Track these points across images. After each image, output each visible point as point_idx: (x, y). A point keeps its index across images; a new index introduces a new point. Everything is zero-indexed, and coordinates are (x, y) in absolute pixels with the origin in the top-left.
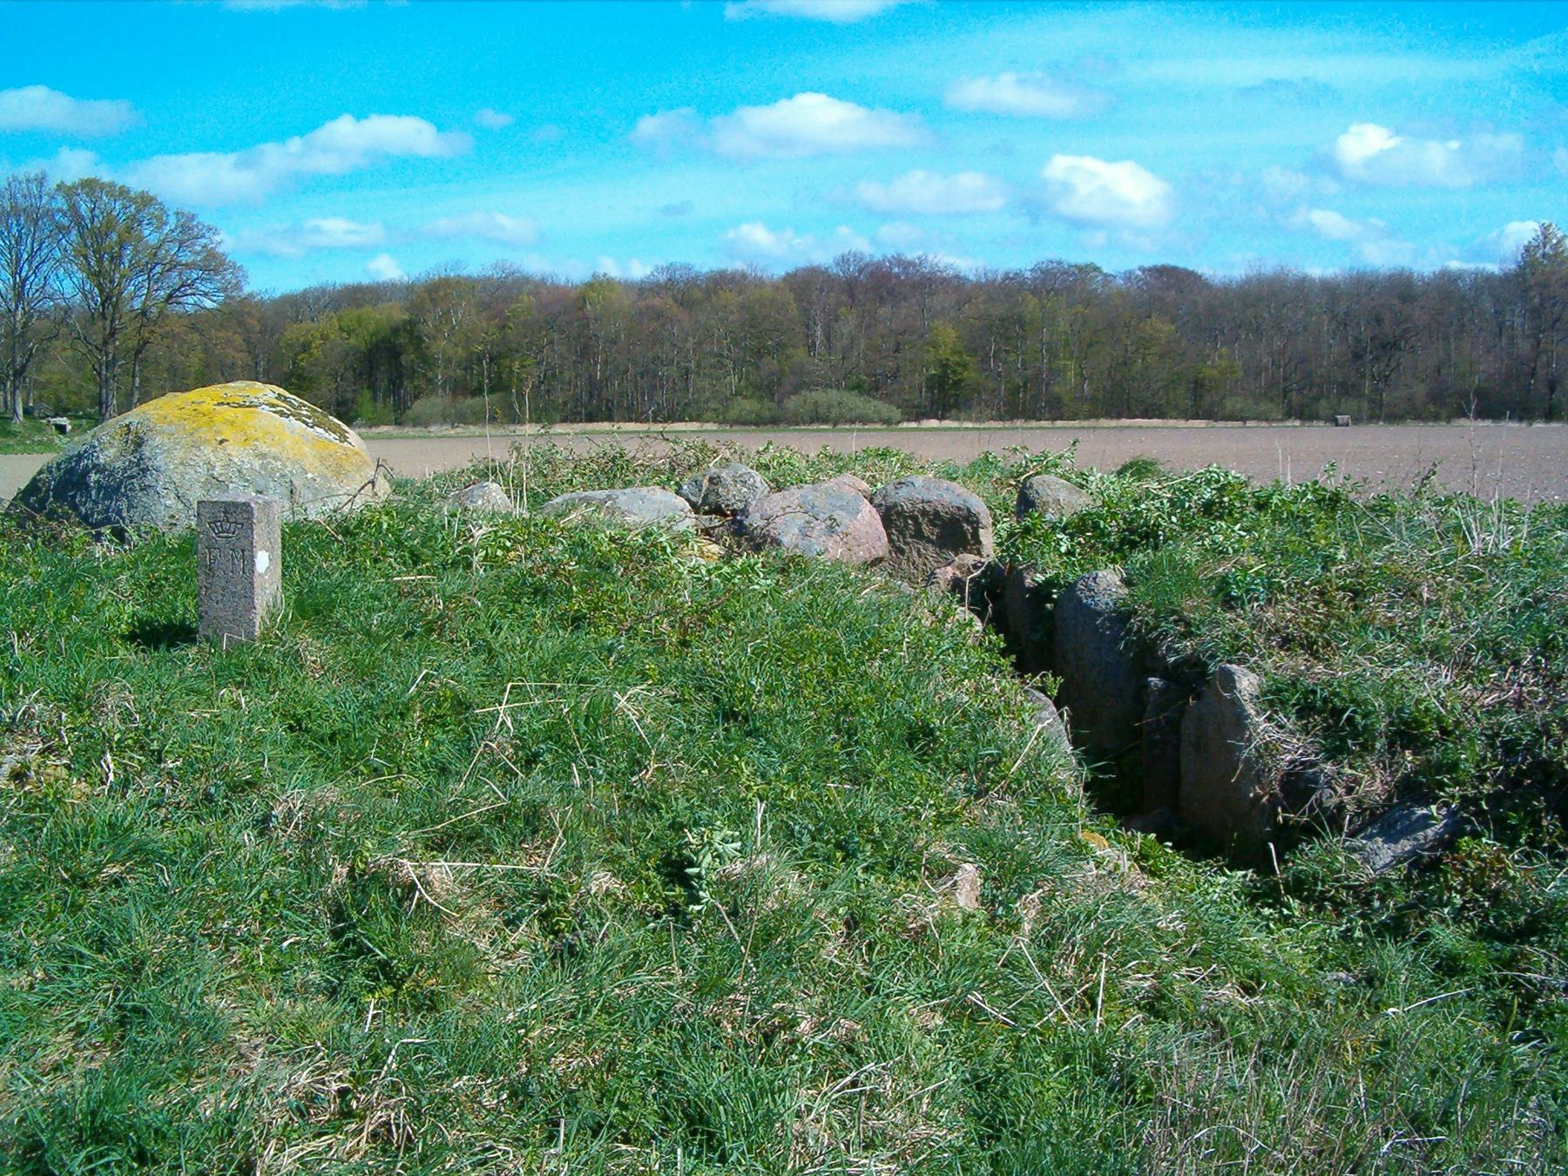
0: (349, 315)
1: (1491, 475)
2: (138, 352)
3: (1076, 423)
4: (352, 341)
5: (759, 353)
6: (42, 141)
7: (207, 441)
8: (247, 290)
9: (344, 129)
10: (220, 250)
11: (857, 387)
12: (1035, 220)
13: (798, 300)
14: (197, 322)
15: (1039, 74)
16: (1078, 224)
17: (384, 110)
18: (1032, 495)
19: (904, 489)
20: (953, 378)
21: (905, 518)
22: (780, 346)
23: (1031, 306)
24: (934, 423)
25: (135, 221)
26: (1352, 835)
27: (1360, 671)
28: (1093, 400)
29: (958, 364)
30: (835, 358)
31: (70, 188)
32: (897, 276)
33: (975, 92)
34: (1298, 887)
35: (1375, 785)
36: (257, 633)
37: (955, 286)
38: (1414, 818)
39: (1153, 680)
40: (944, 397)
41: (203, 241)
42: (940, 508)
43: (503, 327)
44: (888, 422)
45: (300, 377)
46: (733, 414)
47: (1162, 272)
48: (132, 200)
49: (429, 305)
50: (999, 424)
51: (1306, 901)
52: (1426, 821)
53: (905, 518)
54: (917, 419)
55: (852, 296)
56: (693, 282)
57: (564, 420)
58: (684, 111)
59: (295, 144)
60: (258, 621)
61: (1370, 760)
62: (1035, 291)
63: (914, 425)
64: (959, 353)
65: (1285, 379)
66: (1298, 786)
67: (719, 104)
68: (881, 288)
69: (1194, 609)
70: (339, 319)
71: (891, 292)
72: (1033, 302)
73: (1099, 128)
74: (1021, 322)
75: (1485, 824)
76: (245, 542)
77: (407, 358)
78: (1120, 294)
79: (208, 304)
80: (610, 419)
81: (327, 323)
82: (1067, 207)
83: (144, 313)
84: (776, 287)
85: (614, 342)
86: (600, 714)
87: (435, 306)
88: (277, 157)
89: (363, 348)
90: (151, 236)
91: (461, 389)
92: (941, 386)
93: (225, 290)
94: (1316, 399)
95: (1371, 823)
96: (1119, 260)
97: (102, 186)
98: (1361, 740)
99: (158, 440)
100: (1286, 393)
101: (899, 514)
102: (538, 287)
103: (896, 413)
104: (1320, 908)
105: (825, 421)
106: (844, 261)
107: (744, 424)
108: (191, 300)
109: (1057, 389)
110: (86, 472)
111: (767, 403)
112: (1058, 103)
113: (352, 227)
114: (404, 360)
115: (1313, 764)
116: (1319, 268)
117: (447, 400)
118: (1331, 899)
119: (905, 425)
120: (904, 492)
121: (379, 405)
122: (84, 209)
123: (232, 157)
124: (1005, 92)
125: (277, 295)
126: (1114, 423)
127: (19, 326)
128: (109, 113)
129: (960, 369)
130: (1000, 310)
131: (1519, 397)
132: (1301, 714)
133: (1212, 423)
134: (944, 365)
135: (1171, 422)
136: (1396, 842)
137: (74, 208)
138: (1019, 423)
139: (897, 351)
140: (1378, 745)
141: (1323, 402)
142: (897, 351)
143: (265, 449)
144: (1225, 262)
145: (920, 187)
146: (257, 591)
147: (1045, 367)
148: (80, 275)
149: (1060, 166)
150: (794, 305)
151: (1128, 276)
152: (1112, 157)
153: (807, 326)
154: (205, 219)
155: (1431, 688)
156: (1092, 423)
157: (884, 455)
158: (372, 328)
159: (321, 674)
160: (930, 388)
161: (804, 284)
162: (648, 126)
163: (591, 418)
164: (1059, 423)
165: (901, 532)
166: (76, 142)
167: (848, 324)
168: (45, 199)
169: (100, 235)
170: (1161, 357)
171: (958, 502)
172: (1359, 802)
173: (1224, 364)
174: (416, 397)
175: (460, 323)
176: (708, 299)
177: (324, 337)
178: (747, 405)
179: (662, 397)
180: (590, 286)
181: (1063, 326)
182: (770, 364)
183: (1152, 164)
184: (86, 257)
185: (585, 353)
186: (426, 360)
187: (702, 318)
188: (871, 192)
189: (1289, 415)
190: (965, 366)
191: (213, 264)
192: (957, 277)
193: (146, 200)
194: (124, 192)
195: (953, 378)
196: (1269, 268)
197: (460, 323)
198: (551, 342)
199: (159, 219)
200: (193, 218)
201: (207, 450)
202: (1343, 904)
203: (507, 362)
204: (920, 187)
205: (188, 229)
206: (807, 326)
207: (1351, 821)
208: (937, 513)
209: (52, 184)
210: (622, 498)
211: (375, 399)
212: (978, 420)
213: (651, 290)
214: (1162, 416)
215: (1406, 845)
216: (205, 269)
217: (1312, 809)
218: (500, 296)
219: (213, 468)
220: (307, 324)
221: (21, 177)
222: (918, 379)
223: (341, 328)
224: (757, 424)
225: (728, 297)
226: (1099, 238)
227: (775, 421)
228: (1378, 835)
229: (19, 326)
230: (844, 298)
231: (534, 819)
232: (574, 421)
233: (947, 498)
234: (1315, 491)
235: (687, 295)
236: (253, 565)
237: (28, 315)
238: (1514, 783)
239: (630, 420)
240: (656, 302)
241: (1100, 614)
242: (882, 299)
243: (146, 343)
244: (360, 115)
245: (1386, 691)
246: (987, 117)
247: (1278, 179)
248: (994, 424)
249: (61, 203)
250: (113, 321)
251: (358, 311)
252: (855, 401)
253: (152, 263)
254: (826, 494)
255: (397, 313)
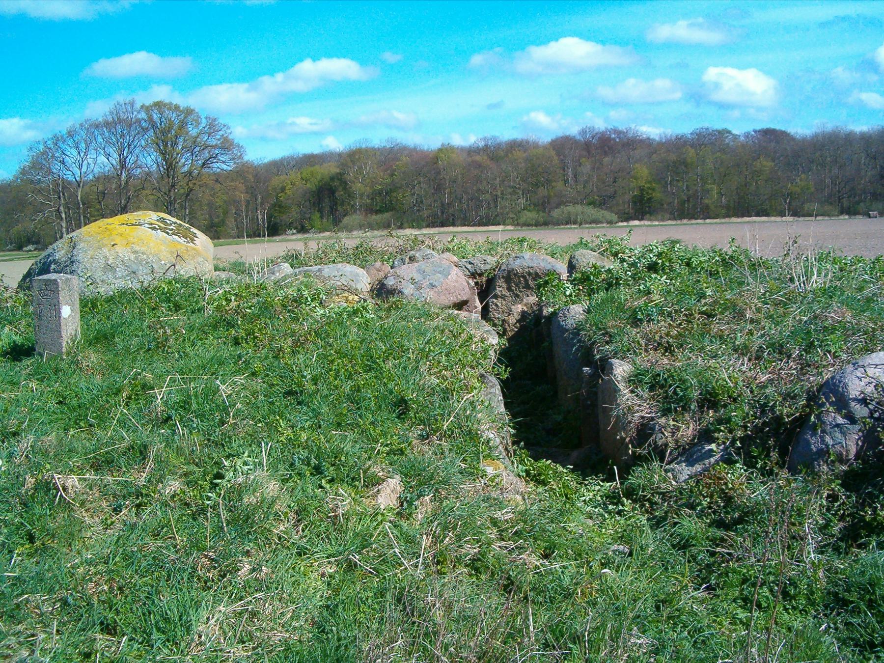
0: (307, 171)
1: (798, 247)
2: (188, 195)
3: (718, 220)
4: (308, 185)
5: (537, 185)
6: (144, 81)
7: (106, 245)
8: (246, 158)
9: (307, 67)
10: (231, 137)
11: (592, 203)
12: (698, 104)
13: (558, 155)
14: (218, 178)
15: (701, 20)
16: (723, 106)
17: (329, 55)
18: (574, 261)
19: (519, 260)
20: (647, 197)
21: (519, 277)
22: (548, 181)
23: (690, 154)
24: (636, 223)
25: (183, 125)
26: (669, 463)
27: (693, 365)
28: (728, 207)
29: (649, 188)
30: (580, 187)
31: (147, 107)
32: (614, 139)
33: (664, 32)
34: (630, 493)
35: (688, 431)
36: (64, 350)
37: (646, 144)
38: (703, 451)
39: (586, 369)
40: (642, 208)
41: (221, 133)
42: (538, 271)
43: (392, 175)
44: (610, 222)
45: (280, 206)
46: (522, 220)
47: (769, 134)
48: (182, 112)
49: (350, 164)
50: (673, 222)
51: (635, 501)
52: (710, 453)
53: (519, 277)
54: (627, 220)
55: (589, 152)
56: (498, 146)
57: (428, 226)
58: (497, 49)
59: (280, 77)
60: (64, 344)
61: (687, 416)
62: (692, 146)
63: (625, 224)
64: (650, 182)
65: (839, 192)
66: (645, 431)
67: (521, 45)
68: (605, 147)
69: (613, 327)
70: (301, 173)
71: (610, 148)
72: (692, 152)
73: (731, 52)
74: (685, 163)
75: (738, 454)
76: (55, 301)
77: (340, 193)
78: (743, 146)
79: (225, 167)
80: (453, 225)
81: (295, 176)
82: (717, 97)
83: (190, 173)
84: (545, 148)
85: (454, 182)
86: (211, 392)
87: (354, 164)
88: (272, 84)
89: (314, 189)
90: (193, 131)
91: (371, 210)
92: (641, 201)
93: (234, 159)
94: (858, 203)
95: (681, 455)
96: (741, 127)
97: (165, 105)
98: (681, 404)
99: (82, 245)
100: (840, 200)
101: (515, 275)
102: (412, 152)
103: (614, 217)
104: (642, 506)
105: (575, 223)
106: (583, 132)
107: (528, 226)
108: (215, 165)
109: (706, 201)
110: (51, 263)
111: (541, 214)
112: (713, 37)
113: (314, 121)
114: (337, 194)
115: (652, 419)
116: (861, 126)
117: (362, 217)
118: (649, 500)
119: (621, 224)
120: (518, 261)
121: (325, 220)
122: (156, 117)
123: (246, 85)
124: (680, 30)
125: (266, 161)
126: (739, 220)
127: (123, 183)
128: (179, 64)
129: (650, 191)
130: (673, 157)
131: (848, 201)
132: (652, 388)
133: (796, 218)
134: (642, 190)
135: (773, 218)
136: (693, 466)
137: (151, 119)
138: (685, 221)
139: (615, 182)
140: (692, 407)
141: (862, 204)
142: (615, 182)
143: (137, 248)
144: (803, 126)
145: (633, 88)
146: (63, 327)
147: (699, 189)
148: (155, 153)
149: (712, 73)
150: (556, 158)
151: (747, 135)
152: (742, 67)
153: (564, 170)
154: (222, 121)
155: (730, 371)
156: (727, 220)
157: (522, 241)
158: (319, 178)
159: (91, 373)
160: (635, 203)
161: (562, 146)
162: (477, 60)
163: (443, 225)
164: (708, 221)
165: (517, 285)
166: (161, 80)
167: (587, 167)
168: (135, 113)
169: (165, 132)
170: (766, 181)
171: (549, 267)
172: (677, 441)
173: (803, 184)
174: (345, 216)
175: (367, 173)
176: (507, 156)
177: (293, 184)
178: (531, 215)
179: (482, 212)
180: (440, 150)
181: (710, 165)
182: (542, 192)
183: (766, 70)
184: (157, 144)
185: (439, 188)
186: (351, 196)
187: (504, 166)
188: (605, 92)
189: (842, 213)
190: (653, 189)
191: (227, 145)
192: (648, 139)
193: (189, 112)
194: (177, 107)
195: (647, 197)
196: (829, 127)
197: (367, 173)
198: (419, 183)
199: (197, 121)
200: (215, 120)
201: (105, 250)
202: (656, 503)
203: (395, 194)
204: (633, 88)
205: (213, 126)
206: (564, 170)
207: (670, 453)
208: (537, 274)
209: (138, 106)
210: (326, 270)
211: (322, 217)
212: (663, 220)
213: (475, 151)
214: (767, 215)
215: (698, 468)
216: (222, 148)
217: (650, 445)
218: (390, 157)
219: (108, 260)
220: (282, 178)
221: (122, 102)
222: (627, 197)
223: (302, 178)
224: (536, 226)
225: (519, 154)
226: (736, 113)
227: (545, 224)
228: (684, 462)
229: (123, 183)
230: (585, 153)
231: (141, 452)
232: (433, 227)
233: (542, 264)
234: (720, 255)
235: (495, 154)
236: (60, 313)
237: (129, 177)
238: (758, 430)
239: (464, 225)
240: (478, 158)
241: (567, 330)
242: (605, 152)
243: (191, 190)
244: (315, 59)
245: (698, 374)
246: (671, 45)
247: (842, 75)
248: (670, 222)
249: (143, 115)
250: (173, 178)
251: (312, 169)
252: (591, 211)
253: (193, 146)
254: (438, 268)
255: (332, 169)
